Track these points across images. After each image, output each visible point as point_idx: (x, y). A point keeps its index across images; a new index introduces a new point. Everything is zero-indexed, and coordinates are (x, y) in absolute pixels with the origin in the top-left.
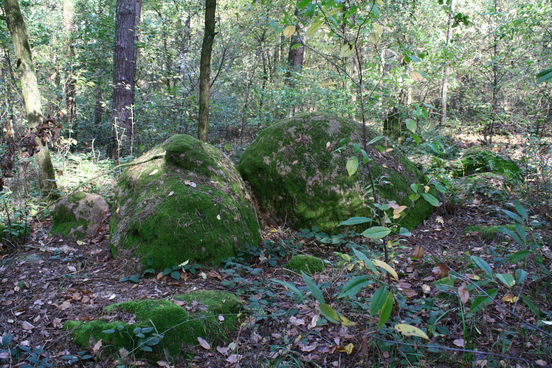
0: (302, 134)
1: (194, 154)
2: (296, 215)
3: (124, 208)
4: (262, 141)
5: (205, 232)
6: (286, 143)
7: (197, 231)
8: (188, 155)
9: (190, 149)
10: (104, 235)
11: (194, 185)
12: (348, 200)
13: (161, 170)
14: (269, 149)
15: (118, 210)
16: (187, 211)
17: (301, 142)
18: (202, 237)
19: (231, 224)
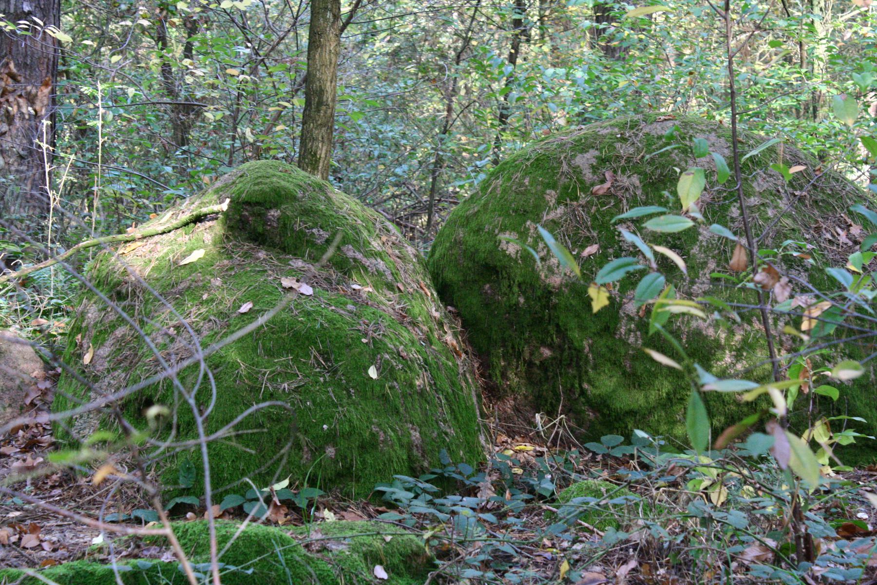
0: (615, 172)
1: (306, 212)
2: (589, 402)
3: (105, 351)
4: (499, 190)
5: (336, 406)
6: (567, 195)
7: (314, 402)
8: (289, 213)
9: (295, 198)
10: (34, 436)
11: (307, 290)
12: (738, 357)
13: (214, 251)
14: (515, 211)
15: (87, 358)
16: (290, 351)
17: (609, 195)
18: (326, 419)
19: (404, 396)
